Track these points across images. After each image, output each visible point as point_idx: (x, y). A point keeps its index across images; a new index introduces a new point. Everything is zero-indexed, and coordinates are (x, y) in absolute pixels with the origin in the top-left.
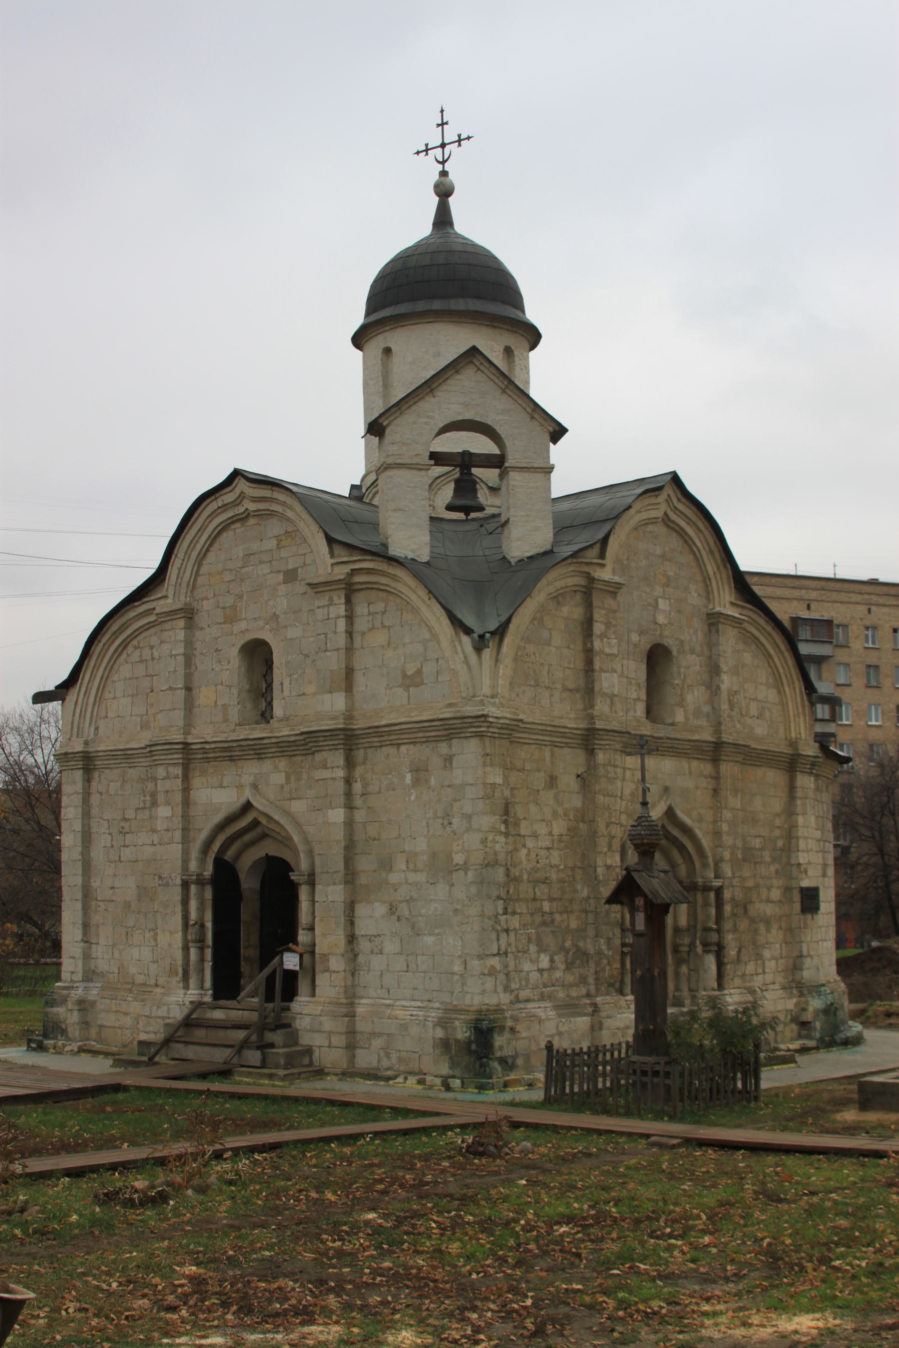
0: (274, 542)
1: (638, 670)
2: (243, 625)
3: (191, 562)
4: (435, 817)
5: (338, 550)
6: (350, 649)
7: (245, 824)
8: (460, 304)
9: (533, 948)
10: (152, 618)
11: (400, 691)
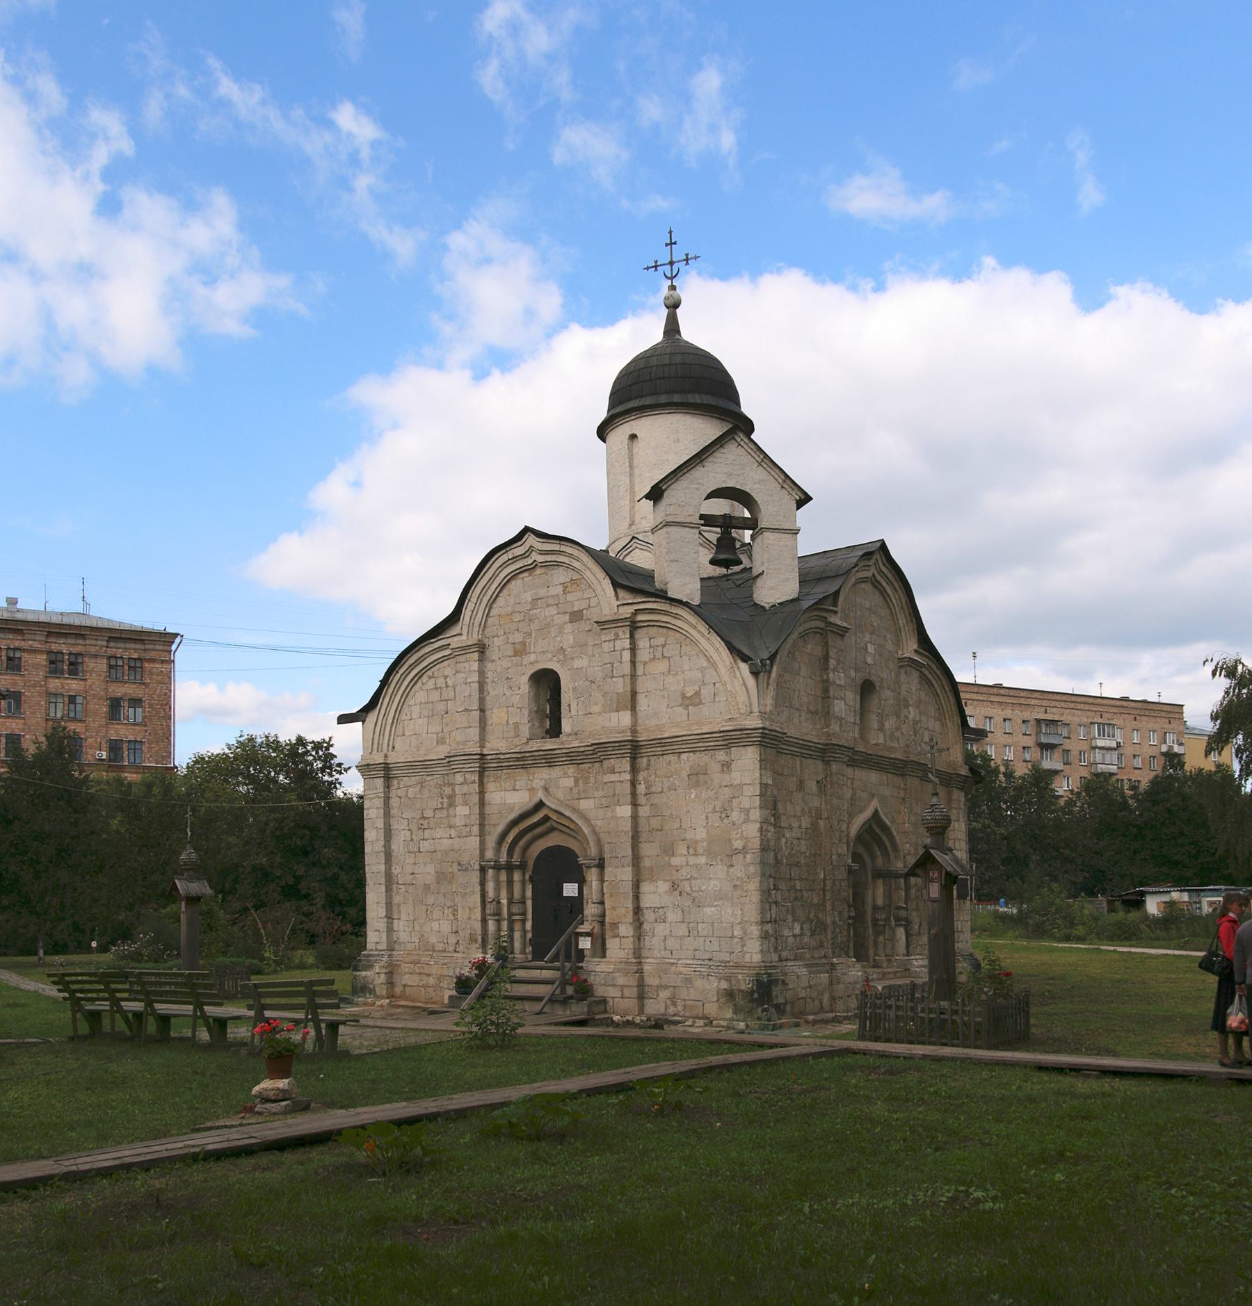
0: (561, 589)
1: (852, 697)
2: (532, 657)
3: (483, 605)
4: (714, 811)
5: (622, 593)
6: (633, 676)
7: (535, 821)
8: (696, 398)
9: (790, 918)
10: (447, 652)
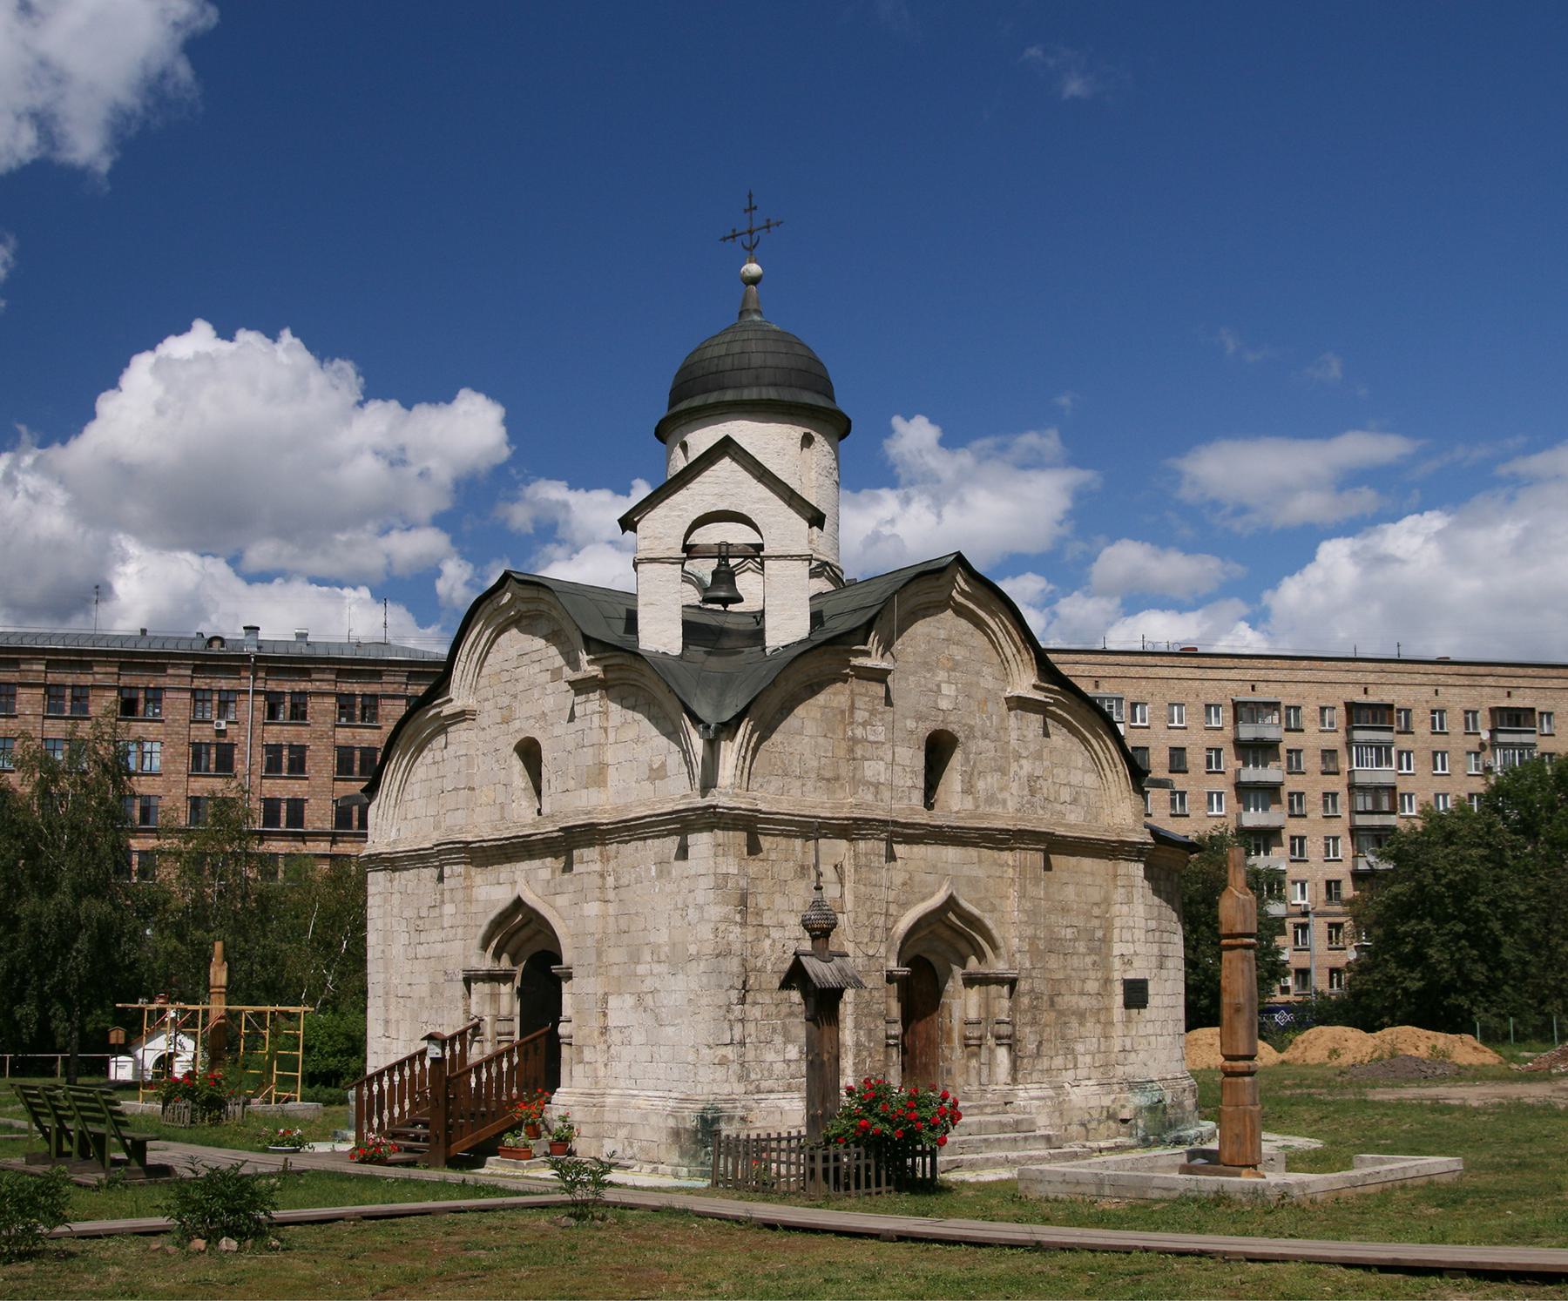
1: (916, 759)
9: (778, 1039)
11: (647, 785)
